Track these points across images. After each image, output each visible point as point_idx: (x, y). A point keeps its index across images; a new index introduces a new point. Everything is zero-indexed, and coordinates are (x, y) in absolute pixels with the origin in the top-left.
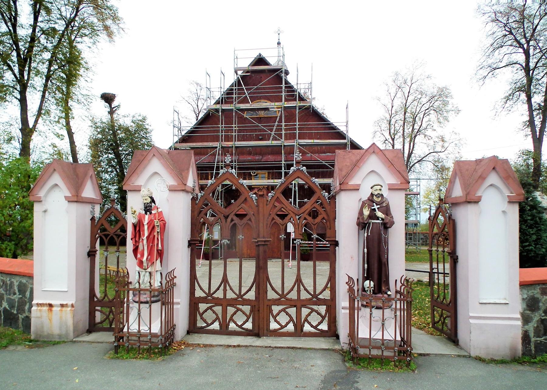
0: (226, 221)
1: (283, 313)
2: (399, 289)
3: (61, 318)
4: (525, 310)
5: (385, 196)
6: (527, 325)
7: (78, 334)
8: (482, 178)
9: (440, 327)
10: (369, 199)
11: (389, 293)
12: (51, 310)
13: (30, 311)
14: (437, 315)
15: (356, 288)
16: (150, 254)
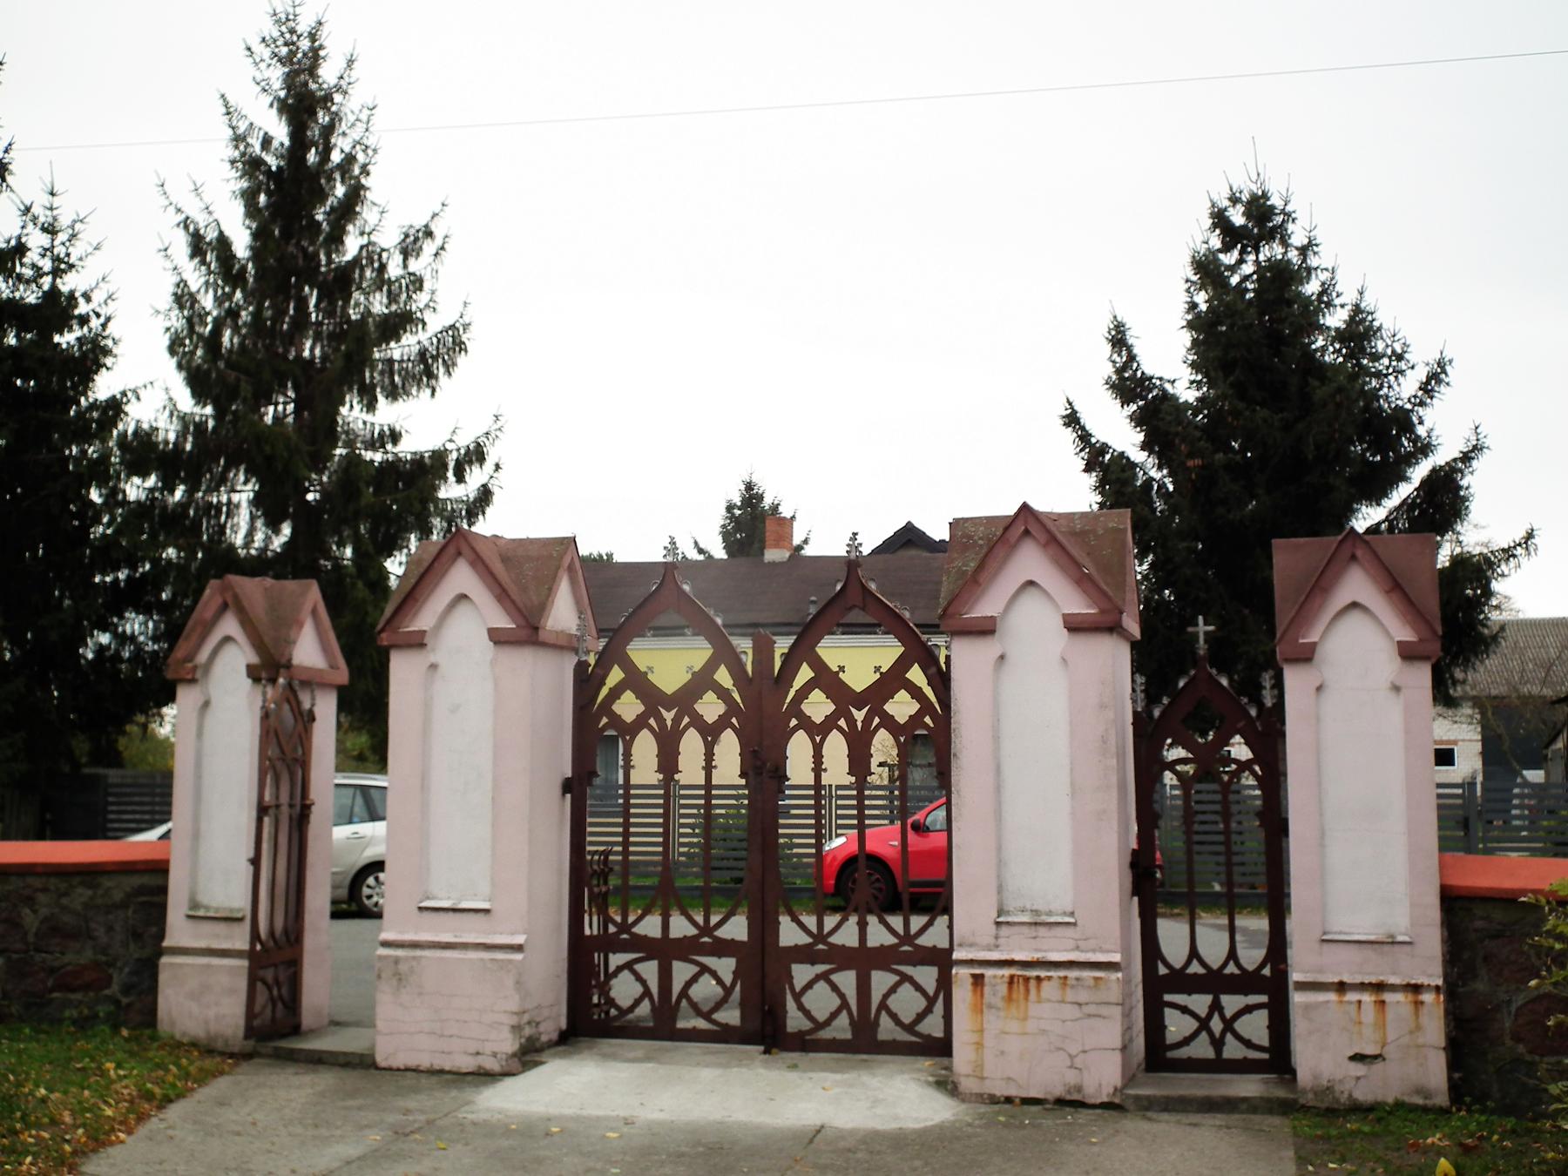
1: (807, 1000)
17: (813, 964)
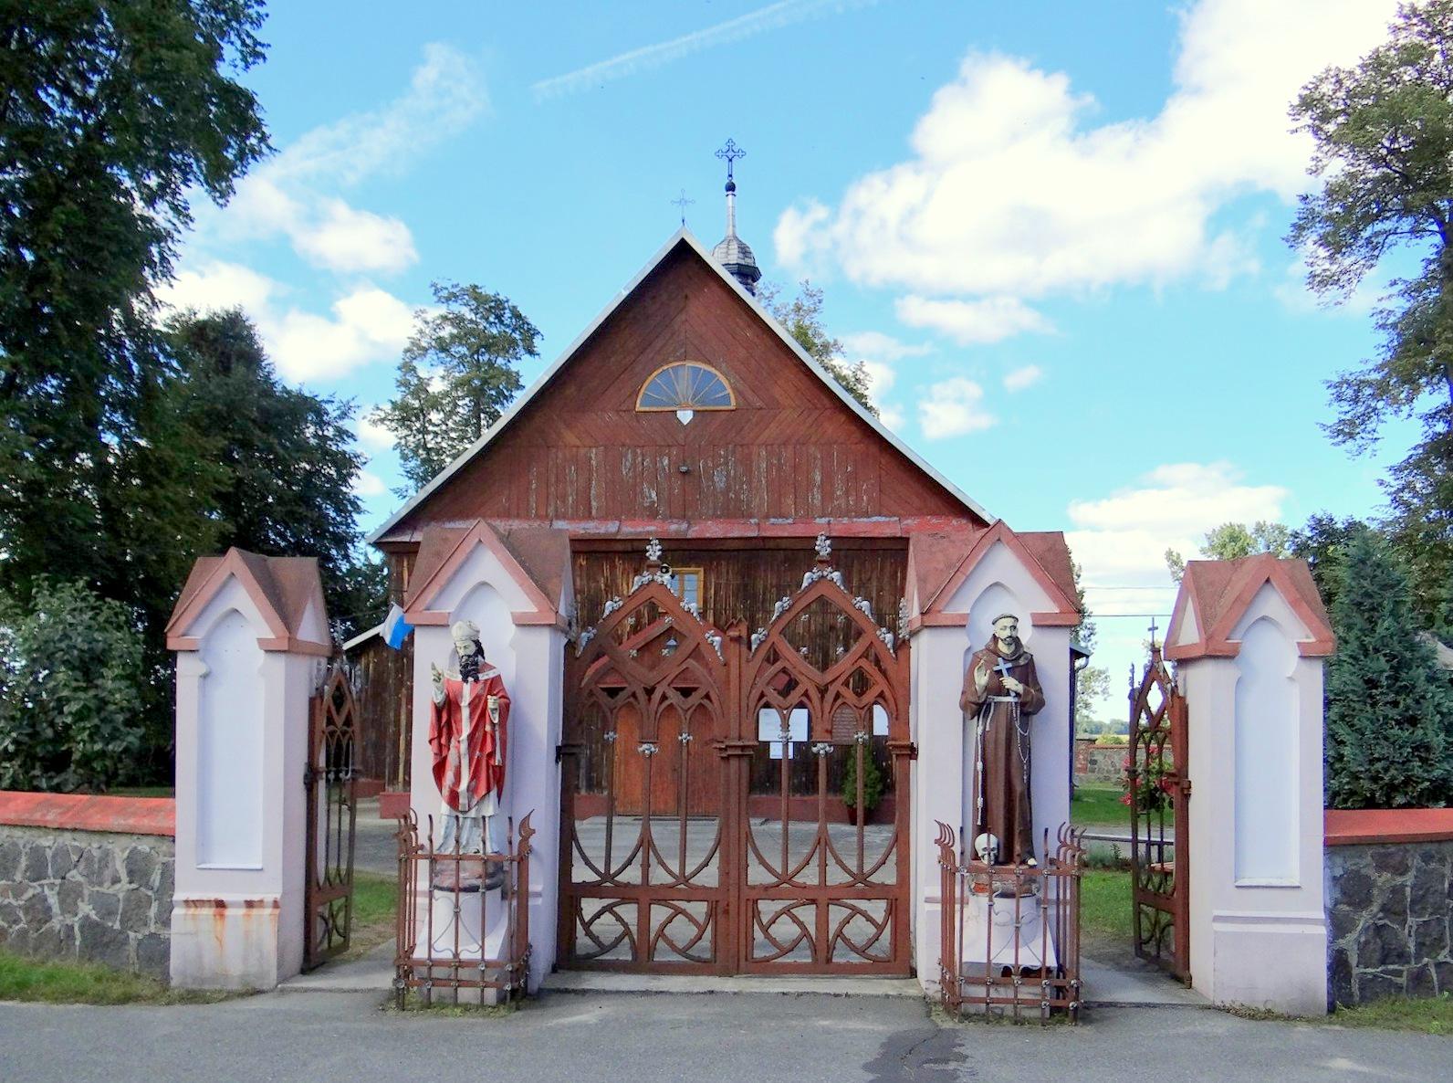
0: (650, 700)
1: (773, 930)
2: (1053, 855)
3: (247, 934)
4: (1336, 903)
5: (1024, 642)
6: (1343, 937)
7: (283, 979)
8: (1245, 603)
9: (1154, 953)
10: (987, 649)
11: (1031, 862)
12: (222, 916)
13: (166, 923)
14: (1145, 924)
15: (957, 849)
16: (475, 776)
17: (601, 898)
